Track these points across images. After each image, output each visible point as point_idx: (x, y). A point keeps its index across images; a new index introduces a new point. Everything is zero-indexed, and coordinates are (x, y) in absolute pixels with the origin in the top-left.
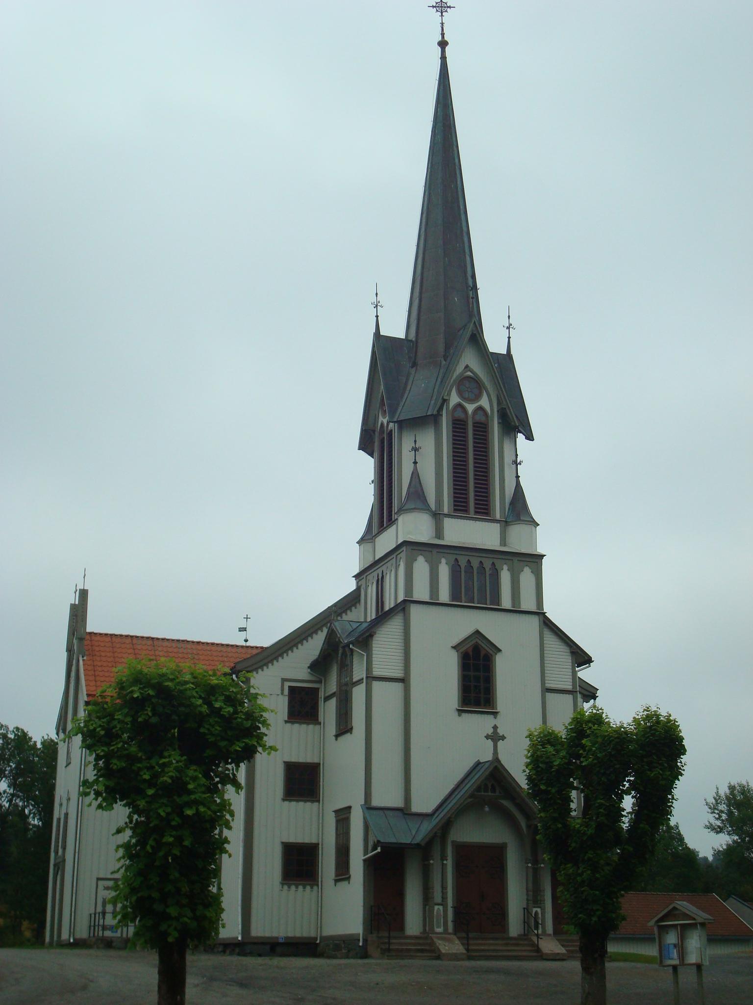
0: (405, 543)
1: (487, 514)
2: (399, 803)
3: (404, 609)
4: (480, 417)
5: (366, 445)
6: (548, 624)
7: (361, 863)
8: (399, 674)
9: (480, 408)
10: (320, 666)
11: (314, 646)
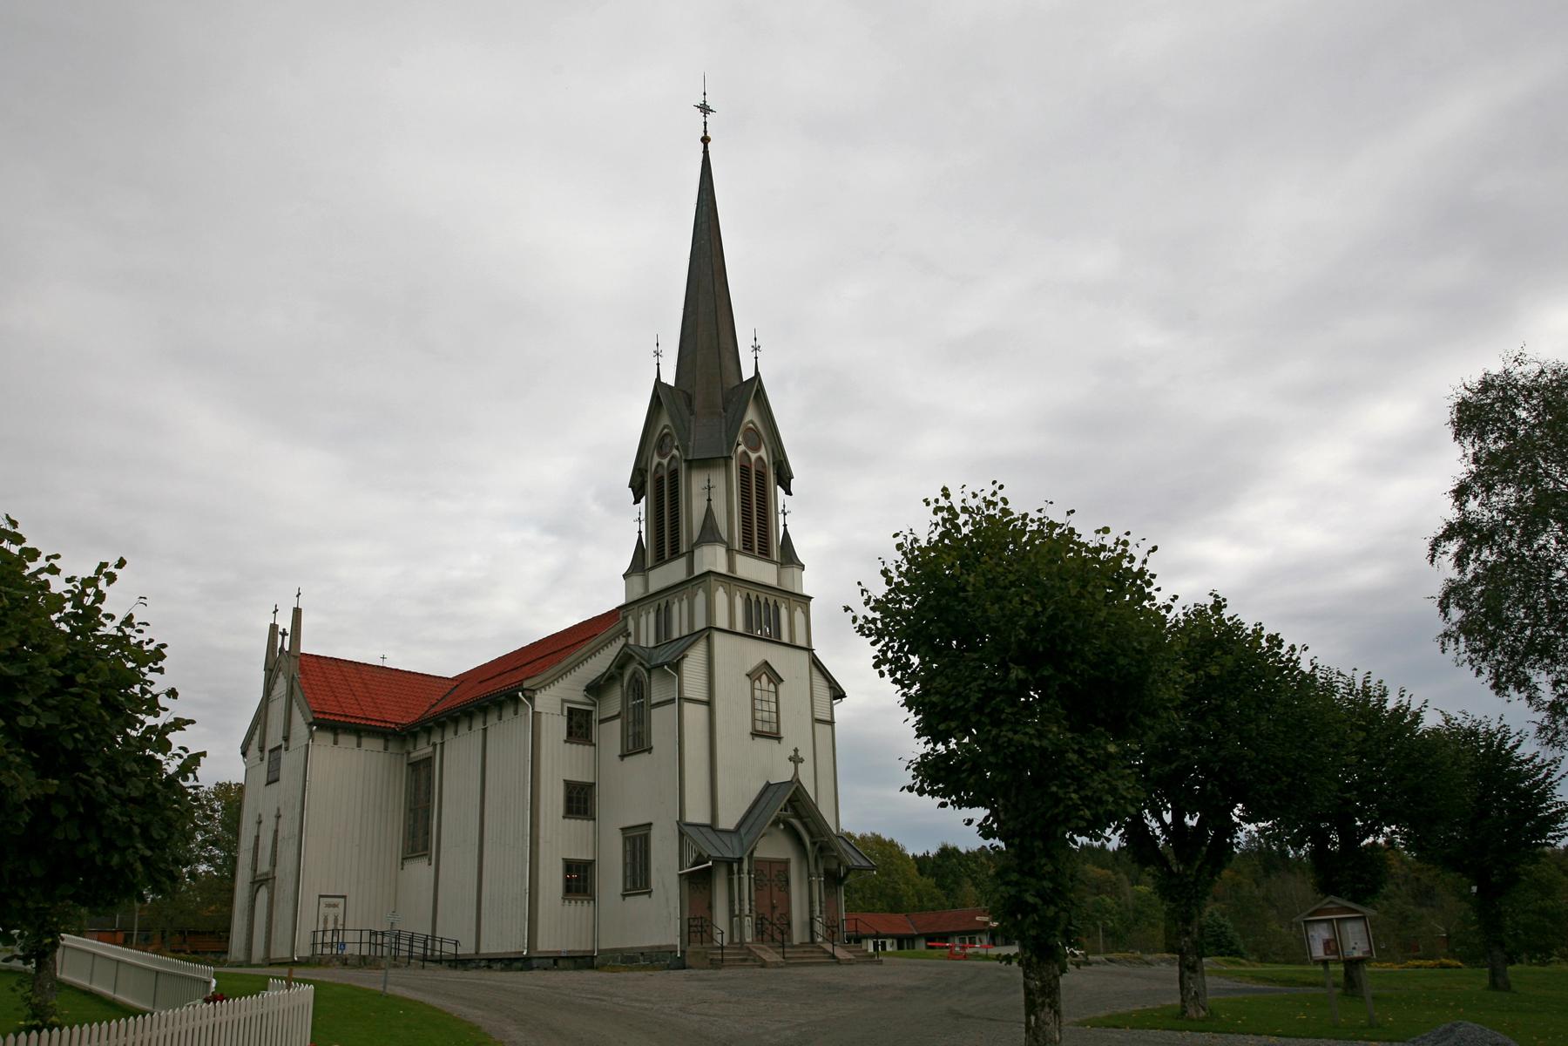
0: (709, 573)
2: (706, 820)
3: (708, 638)
6: (816, 663)
7: (676, 879)
8: (704, 697)
9: (760, 458)
10: (596, 689)
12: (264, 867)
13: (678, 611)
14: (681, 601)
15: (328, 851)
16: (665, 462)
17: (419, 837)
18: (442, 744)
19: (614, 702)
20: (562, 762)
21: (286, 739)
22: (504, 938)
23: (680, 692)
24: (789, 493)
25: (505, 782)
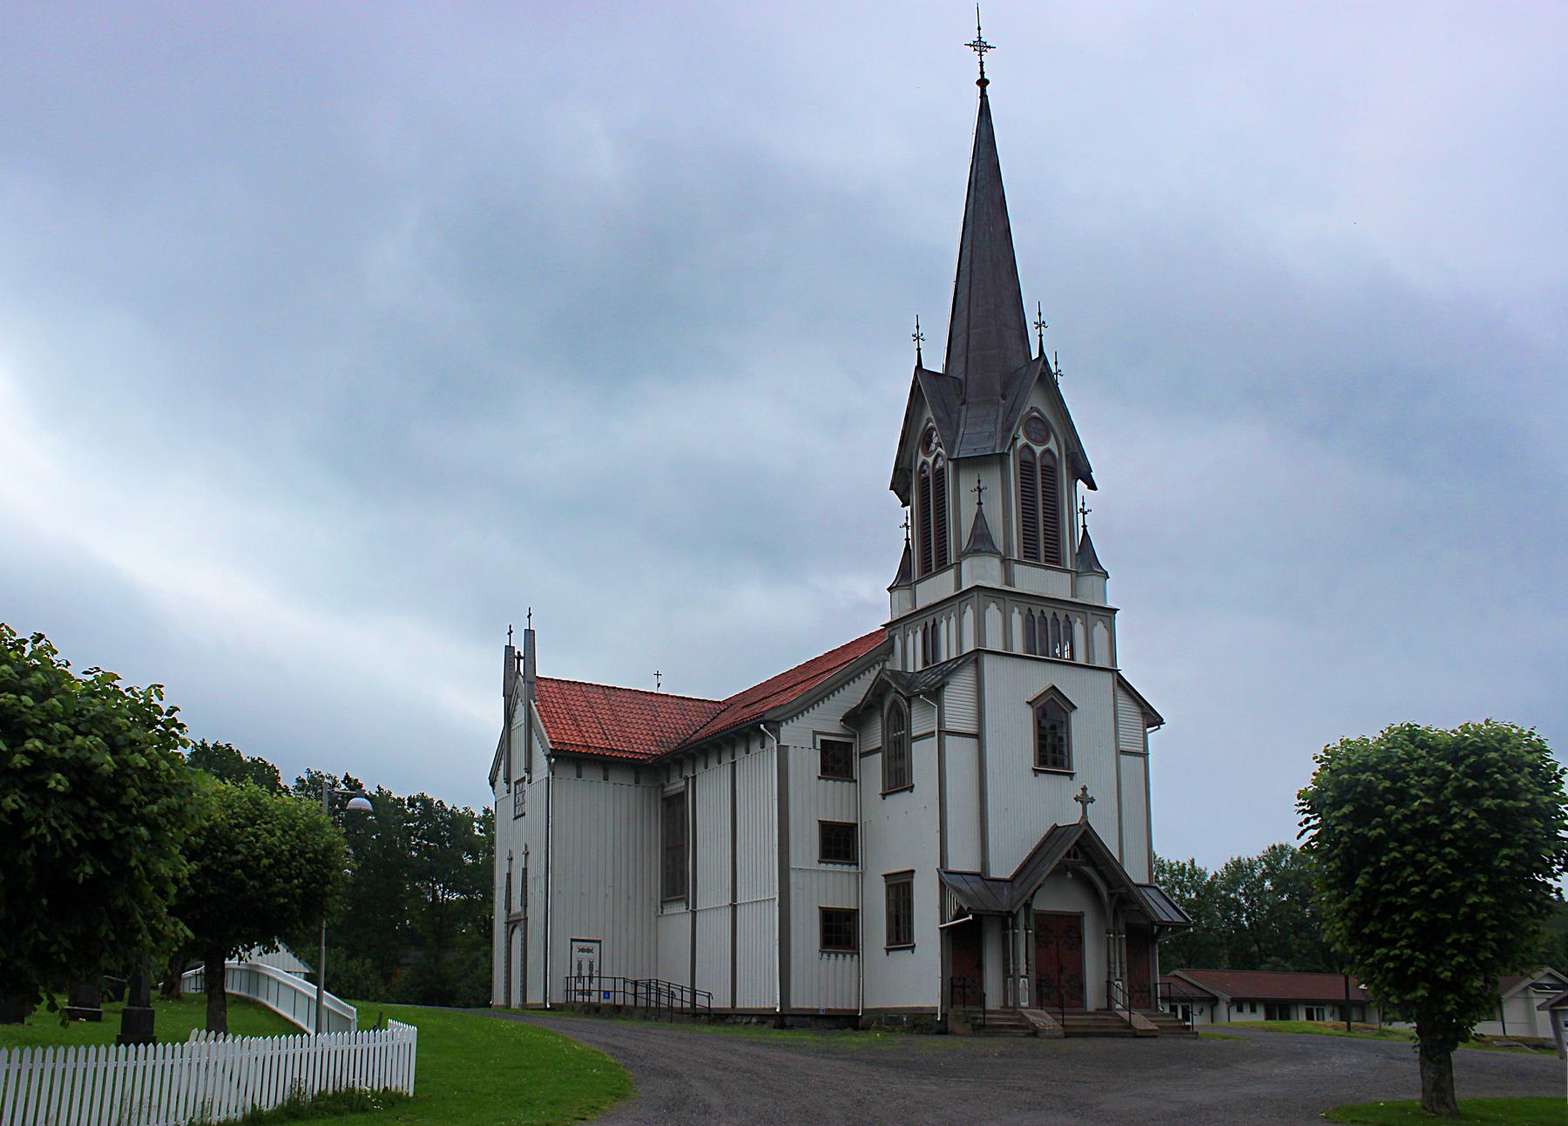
0: (977, 588)
1: (1058, 563)
2: (977, 870)
3: (976, 661)
4: (1048, 460)
5: (900, 484)
6: (1122, 684)
7: (938, 933)
8: (973, 730)
9: (1048, 451)
10: (855, 719)
11: (855, 693)
12: (517, 907)
13: (946, 632)
14: (948, 619)
15: (564, 890)
16: (930, 460)
17: (676, 882)
18: (694, 778)
19: (875, 736)
20: (819, 801)
21: (529, 770)
22: (761, 993)
23: (941, 722)
24: (1092, 486)
25: (747, 817)
